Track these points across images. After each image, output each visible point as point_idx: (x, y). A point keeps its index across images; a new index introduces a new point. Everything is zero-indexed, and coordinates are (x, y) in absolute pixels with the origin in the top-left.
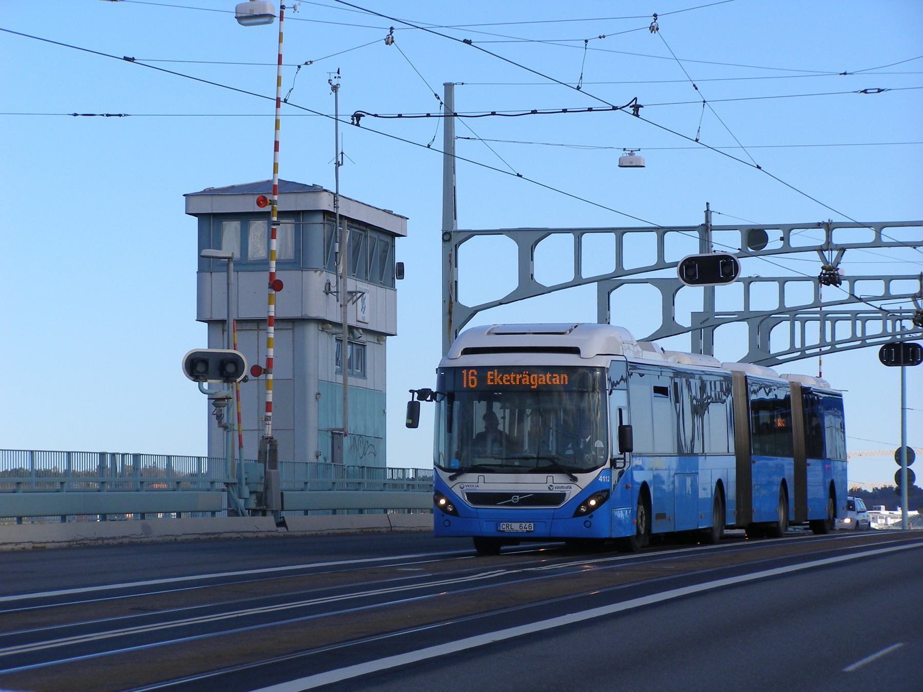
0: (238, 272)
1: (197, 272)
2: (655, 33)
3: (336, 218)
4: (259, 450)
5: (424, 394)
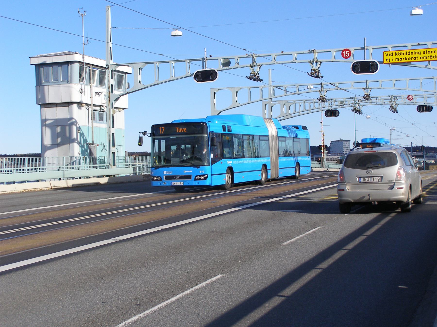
0: (39, 86)
1: (36, 86)
2: (405, 57)
3: (83, 64)
5: (144, 133)
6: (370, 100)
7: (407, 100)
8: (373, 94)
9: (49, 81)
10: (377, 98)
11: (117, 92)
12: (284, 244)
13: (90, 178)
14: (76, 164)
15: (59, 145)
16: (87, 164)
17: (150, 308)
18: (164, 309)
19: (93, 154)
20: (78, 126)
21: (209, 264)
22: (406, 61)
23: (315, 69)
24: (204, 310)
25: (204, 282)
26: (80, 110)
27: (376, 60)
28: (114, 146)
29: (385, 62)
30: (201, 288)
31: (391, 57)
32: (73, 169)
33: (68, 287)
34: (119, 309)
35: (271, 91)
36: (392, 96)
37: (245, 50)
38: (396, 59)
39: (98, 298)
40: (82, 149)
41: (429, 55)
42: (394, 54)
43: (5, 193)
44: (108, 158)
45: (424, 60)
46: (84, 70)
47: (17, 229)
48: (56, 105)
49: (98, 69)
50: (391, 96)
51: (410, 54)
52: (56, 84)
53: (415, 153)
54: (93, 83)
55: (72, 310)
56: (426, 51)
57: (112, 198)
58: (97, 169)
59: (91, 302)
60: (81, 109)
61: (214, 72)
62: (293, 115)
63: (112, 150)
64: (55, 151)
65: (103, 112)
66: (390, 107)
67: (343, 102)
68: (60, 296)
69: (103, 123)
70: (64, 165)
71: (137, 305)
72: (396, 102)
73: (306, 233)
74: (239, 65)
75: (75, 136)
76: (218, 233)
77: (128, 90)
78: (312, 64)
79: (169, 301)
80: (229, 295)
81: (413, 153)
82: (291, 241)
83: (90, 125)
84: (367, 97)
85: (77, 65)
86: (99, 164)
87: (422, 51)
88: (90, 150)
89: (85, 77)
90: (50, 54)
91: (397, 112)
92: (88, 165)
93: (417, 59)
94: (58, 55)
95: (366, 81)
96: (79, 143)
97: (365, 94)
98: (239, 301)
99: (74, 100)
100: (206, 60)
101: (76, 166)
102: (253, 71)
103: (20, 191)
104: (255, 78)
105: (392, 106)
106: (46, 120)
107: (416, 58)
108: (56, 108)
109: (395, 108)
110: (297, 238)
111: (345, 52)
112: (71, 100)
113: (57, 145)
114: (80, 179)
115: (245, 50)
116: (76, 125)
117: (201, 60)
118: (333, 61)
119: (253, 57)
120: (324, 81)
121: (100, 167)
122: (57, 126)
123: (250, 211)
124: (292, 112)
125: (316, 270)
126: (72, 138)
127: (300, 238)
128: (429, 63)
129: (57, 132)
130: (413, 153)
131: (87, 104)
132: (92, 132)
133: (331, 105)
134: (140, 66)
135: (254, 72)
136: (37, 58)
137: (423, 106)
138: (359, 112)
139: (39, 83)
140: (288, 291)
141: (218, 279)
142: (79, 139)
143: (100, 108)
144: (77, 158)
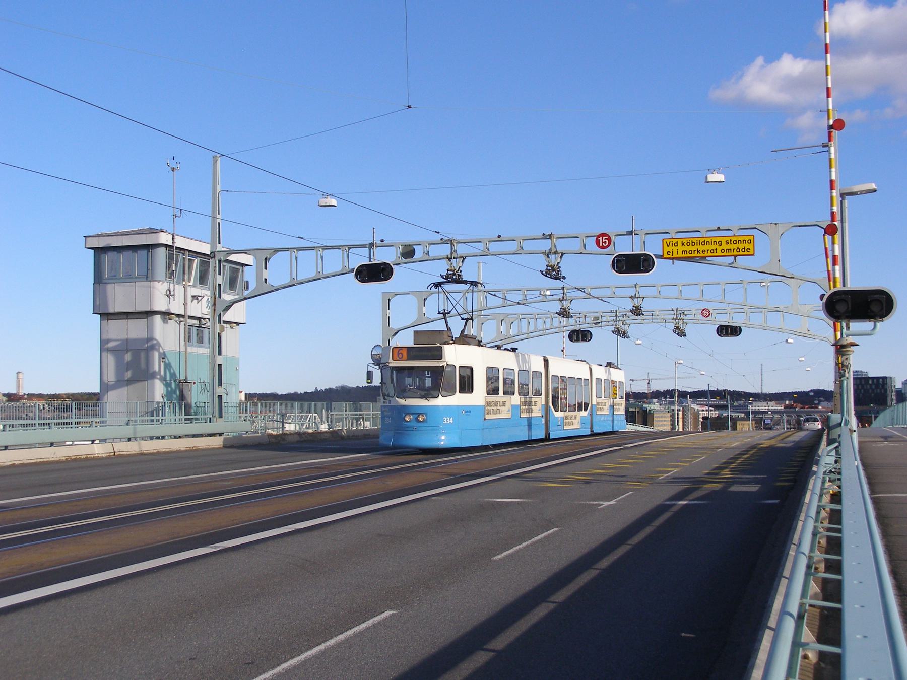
3: (173, 248)
4: (813, 532)
6: (641, 315)
7: (701, 317)
8: (645, 306)
9: (115, 276)
10: (653, 312)
11: (227, 297)
12: (496, 558)
13: (180, 437)
14: (158, 415)
15: (130, 382)
16: (175, 415)
17: (269, 670)
18: (293, 670)
19: (185, 398)
20: (161, 351)
21: (370, 592)
22: (699, 255)
24: (359, 674)
25: (362, 625)
26: (166, 325)
27: (651, 253)
28: (221, 386)
29: (666, 256)
30: (356, 635)
31: (675, 249)
32: (153, 423)
33: (134, 630)
34: (218, 671)
35: (482, 298)
36: (677, 309)
37: (438, 233)
38: (683, 251)
39: (184, 650)
40: (167, 390)
41: (735, 246)
42: (680, 244)
43: (36, 462)
44: (209, 405)
45: (728, 254)
46: (175, 260)
47: (53, 527)
49: (198, 258)
50: (675, 310)
51: (704, 245)
52: (127, 280)
53: (715, 401)
54: (189, 281)
55: (138, 672)
56: (731, 241)
57: (219, 473)
58: (191, 423)
59: (171, 658)
60: (167, 323)
61: (388, 268)
62: (517, 338)
63: (217, 391)
64: (123, 391)
65: (205, 328)
67: (599, 317)
68: (118, 646)
69: (204, 347)
70: (137, 416)
71: (249, 664)
72: (683, 319)
73: (533, 540)
74: (429, 256)
75: (156, 368)
76: (389, 537)
77: (246, 293)
78: (548, 257)
79: (302, 657)
80: (402, 647)
81: (712, 401)
82: (507, 552)
83: (183, 349)
84: (637, 311)
85: (162, 250)
86: (196, 415)
87: (724, 240)
88: (182, 392)
89: (176, 271)
90: (119, 232)
91: (685, 335)
92: (177, 417)
93: (716, 252)
94: (132, 233)
95: (636, 285)
96: (163, 379)
97: (633, 306)
98: (419, 658)
99: (157, 309)
100: (375, 246)
101: (158, 418)
102: (451, 267)
103: (61, 459)
104: (454, 277)
105: (677, 325)
106: (108, 341)
107: (715, 251)
108: (126, 320)
109: (682, 329)
110: (518, 547)
111: (601, 239)
112: (152, 309)
113: (126, 382)
114: (163, 440)
115: (438, 233)
116: (158, 350)
117: (367, 246)
118: (581, 253)
119: (452, 244)
120: (569, 282)
121: (197, 419)
122: (127, 350)
123: (441, 500)
124: (516, 333)
125: (547, 604)
126: (151, 371)
127: (524, 547)
128: (735, 259)
129: (126, 361)
130: (712, 401)
131: (178, 316)
132: (186, 361)
133: (578, 322)
134: (267, 254)
135: (453, 268)
136: (97, 238)
137: (727, 327)
138: (624, 335)
139: (99, 279)
140: (500, 642)
141: (385, 619)
142: (162, 373)
143: (200, 322)
144: (159, 404)
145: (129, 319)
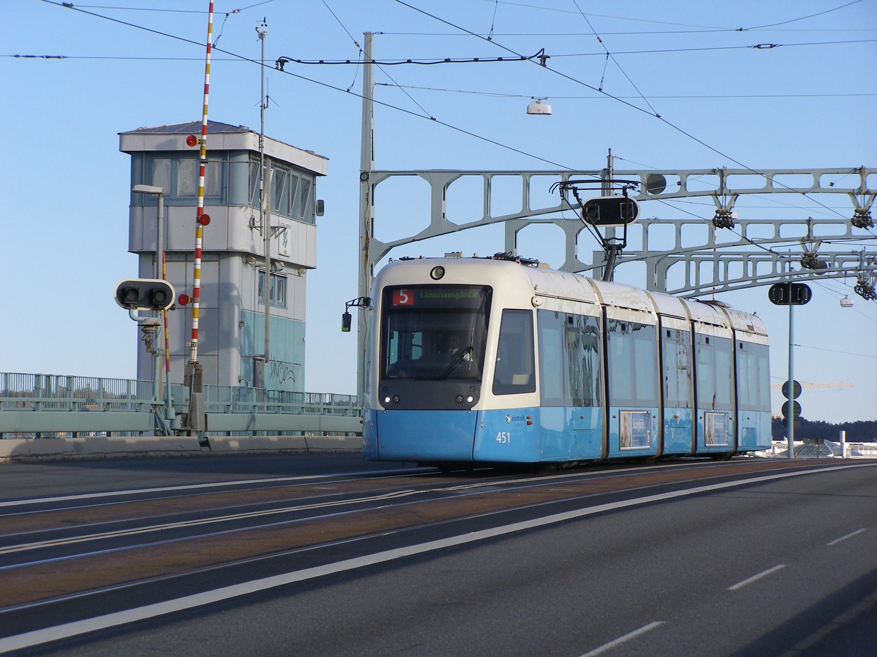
0: (143, 207)
1: (130, 206)
23: (864, 210)
37: (69, 6)
48: (184, 255)
66: (857, 284)
112: (231, 247)
115: (69, 6)
117: (601, 173)
134: (447, 177)
145: (188, 261)
